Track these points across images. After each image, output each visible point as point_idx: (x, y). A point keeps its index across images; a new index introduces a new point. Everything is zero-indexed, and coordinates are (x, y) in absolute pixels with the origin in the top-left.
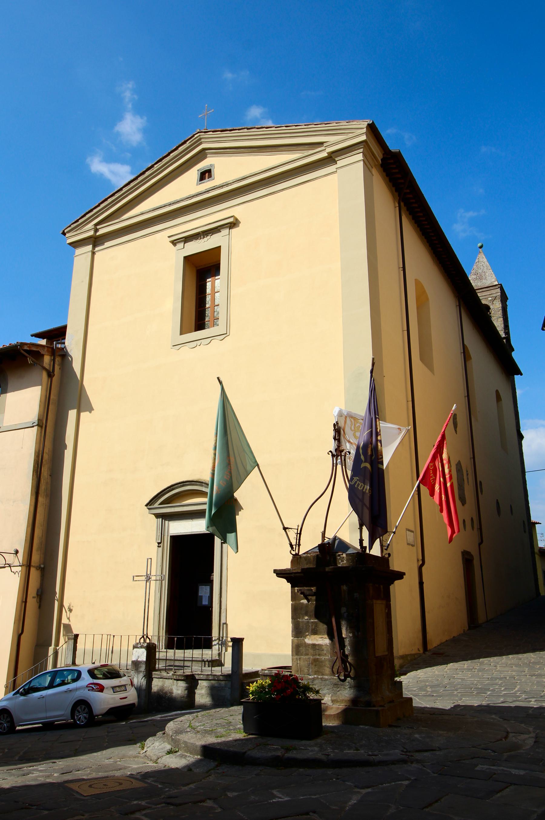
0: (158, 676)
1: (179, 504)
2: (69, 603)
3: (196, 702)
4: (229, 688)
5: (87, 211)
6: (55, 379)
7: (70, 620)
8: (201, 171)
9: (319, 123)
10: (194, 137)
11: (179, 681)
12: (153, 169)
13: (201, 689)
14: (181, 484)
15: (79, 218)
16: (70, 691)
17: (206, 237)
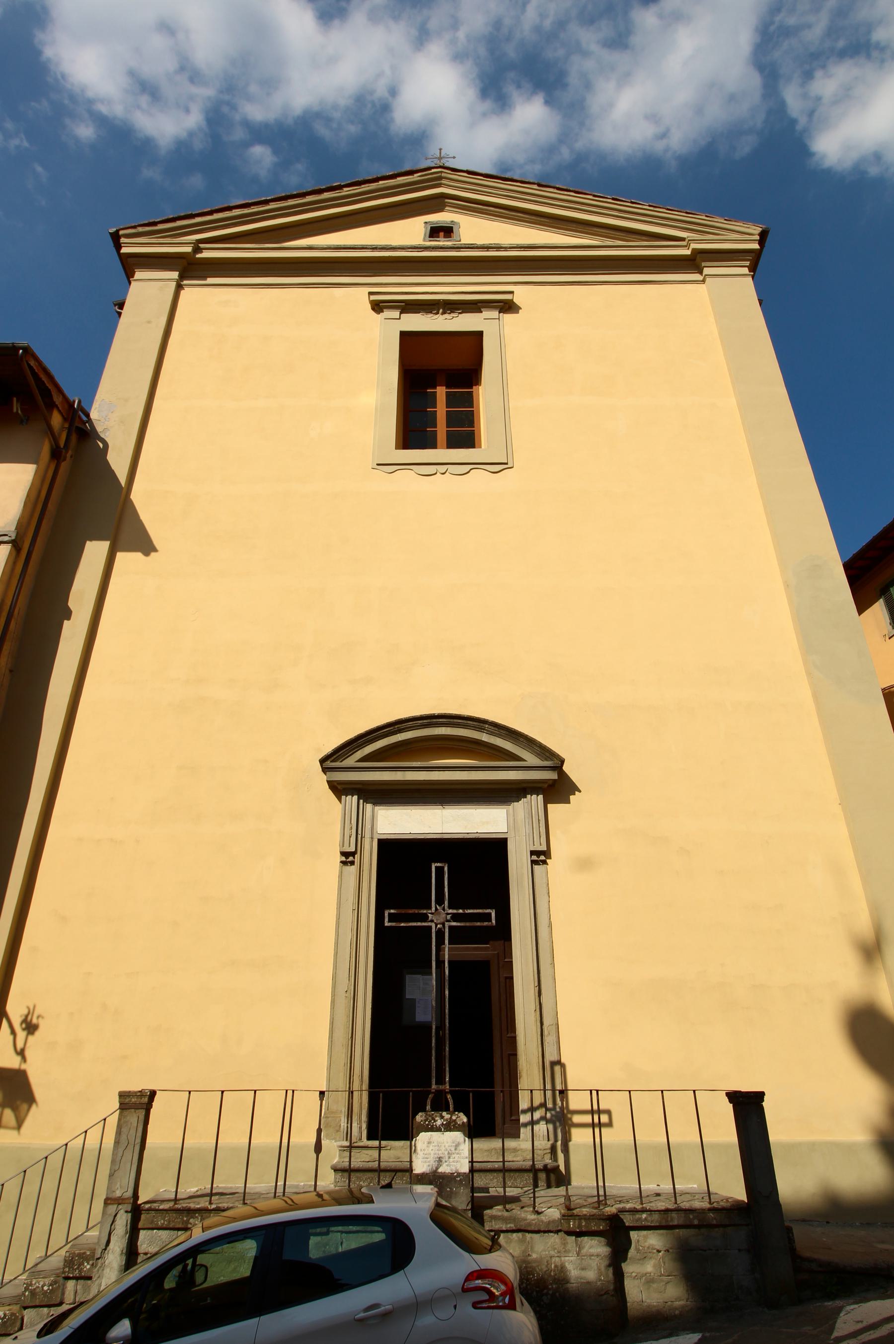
0: (507, 1223)
1: (419, 763)
2: (28, 1008)
3: (628, 1304)
4: (739, 1250)
5: (182, 214)
6: (65, 466)
7: (24, 1059)
8: (433, 226)
9: (676, 209)
10: (431, 172)
11: (586, 1239)
12: (340, 192)
13: (639, 1260)
14: (425, 721)
15: (159, 220)
16: (386, 1315)
17: (449, 313)
